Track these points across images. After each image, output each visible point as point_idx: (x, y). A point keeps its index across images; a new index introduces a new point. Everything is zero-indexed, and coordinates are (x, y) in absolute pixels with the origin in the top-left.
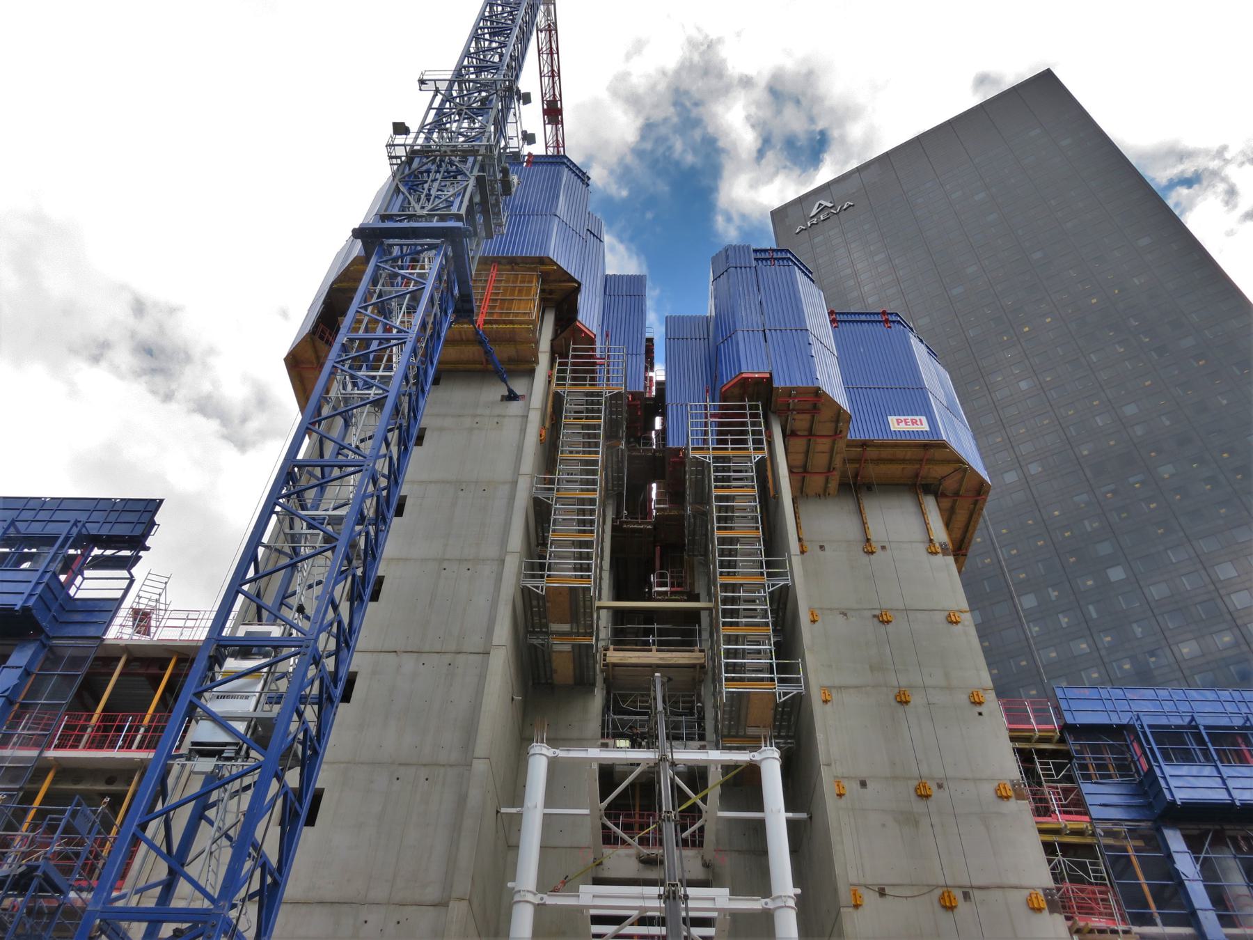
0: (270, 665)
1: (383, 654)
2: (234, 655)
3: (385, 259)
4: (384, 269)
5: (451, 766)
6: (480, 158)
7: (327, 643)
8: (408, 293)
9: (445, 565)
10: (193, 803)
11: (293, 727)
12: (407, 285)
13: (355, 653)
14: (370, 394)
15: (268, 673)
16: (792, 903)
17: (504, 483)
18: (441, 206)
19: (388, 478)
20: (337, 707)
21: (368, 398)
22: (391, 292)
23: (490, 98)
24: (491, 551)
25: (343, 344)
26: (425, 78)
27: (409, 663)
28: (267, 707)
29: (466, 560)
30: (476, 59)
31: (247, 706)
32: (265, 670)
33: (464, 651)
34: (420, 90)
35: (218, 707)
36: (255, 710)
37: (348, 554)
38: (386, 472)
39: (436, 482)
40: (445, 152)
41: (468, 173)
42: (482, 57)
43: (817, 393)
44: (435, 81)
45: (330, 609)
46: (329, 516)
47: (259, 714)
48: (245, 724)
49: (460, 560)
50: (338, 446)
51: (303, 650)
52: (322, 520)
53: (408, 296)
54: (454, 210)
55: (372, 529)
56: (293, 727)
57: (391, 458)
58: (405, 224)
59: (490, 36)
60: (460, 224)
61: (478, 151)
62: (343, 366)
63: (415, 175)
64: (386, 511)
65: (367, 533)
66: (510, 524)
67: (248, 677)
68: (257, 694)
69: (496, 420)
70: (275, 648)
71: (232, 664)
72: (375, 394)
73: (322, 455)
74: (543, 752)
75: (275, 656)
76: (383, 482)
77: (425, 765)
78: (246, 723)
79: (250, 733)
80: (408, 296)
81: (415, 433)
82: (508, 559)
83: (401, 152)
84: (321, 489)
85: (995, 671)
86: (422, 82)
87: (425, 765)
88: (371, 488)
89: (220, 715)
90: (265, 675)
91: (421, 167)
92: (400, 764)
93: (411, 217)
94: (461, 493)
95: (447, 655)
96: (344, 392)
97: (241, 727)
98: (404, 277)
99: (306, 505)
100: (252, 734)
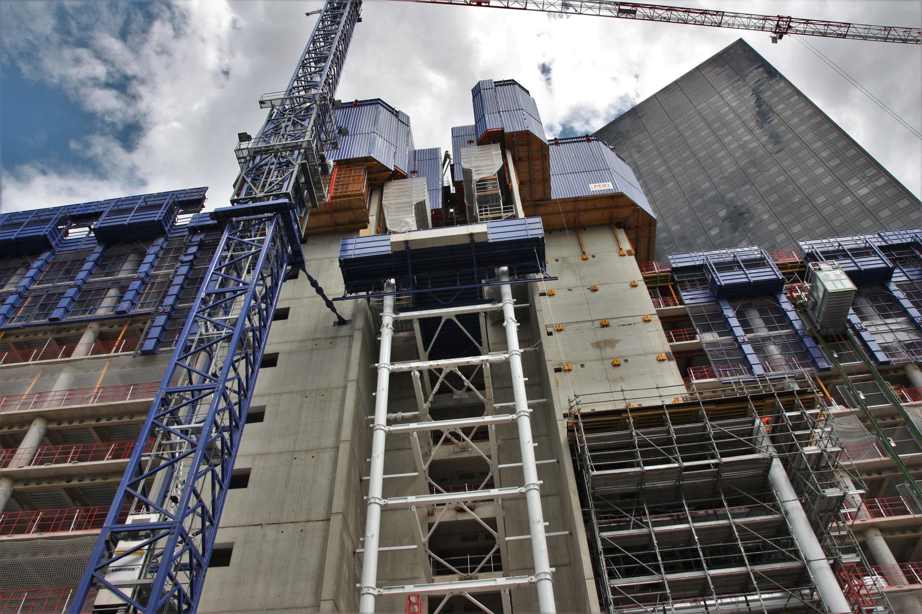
0: (150, 543)
1: (251, 527)
2: (125, 539)
3: (234, 232)
4: (234, 239)
5: (306, 607)
6: (302, 151)
7: (192, 523)
8: (250, 255)
9: (296, 455)
11: (168, 587)
12: (251, 249)
13: (219, 530)
14: (222, 333)
15: (149, 550)
17: (337, 388)
18: (275, 188)
20: (206, 571)
21: (220, 336)
22: (241, 255)
23: (312, 107)
24: (329, 441)
25: (202, 299)
26: (264, 99)
27: (271, 532)
28: (149, 576)
29: (311, 450)
30: (305, 81)
31: (132, 576)
32: (146, 547)
34: (261, 108)
35: (111, 578)
36: (139, 578)
37: (205, 454)
38: (236, 388)
39: (287, 393)
40: (278, 149)
41: (294, 163)
42: (309, 79)
44: (271, 101)
45: (193, 497)
46: (191, 428)
47: (142, 581)
48: (132, 589)
49: (306, 450)
50: (203, 377)
51: (172, 531)
53: (250, 257)
54: (284, 190)
56: (168, 587)
57: (239, 380)
58: (251, 204)
59: (315, 64)
60: (286, 200)
61: (301, 146)
62: (204, 314)
63: (259, 169)
66: (342, 419)
67: (134, 553)
68: (141, 566)
69: (330, 341)
70: (153, 530)
71: (123, 545)
72: (226, 333)
73: (191, 382)
74: (370, 592)
75: (153, 537)
76: (234, 398)
77: (286, 609)
78: (132, 589)
79: (136, 596)
80: (250, 257)
82: (342, 446)
83: (245, 153)
84: (193, 406)
85: (374, 394)
86: (262, 102)
87: (286, 609)
88: (223, 404)
89: (113, 584)
90: (146, 551)
91: (261, 162)
92: (268, 610)
93: (255, 200)
94: (306, 400)
95: (299, 524)
97: (128, 592)
98: (247, 244)
99: (180, 421)
100: (138, 597)
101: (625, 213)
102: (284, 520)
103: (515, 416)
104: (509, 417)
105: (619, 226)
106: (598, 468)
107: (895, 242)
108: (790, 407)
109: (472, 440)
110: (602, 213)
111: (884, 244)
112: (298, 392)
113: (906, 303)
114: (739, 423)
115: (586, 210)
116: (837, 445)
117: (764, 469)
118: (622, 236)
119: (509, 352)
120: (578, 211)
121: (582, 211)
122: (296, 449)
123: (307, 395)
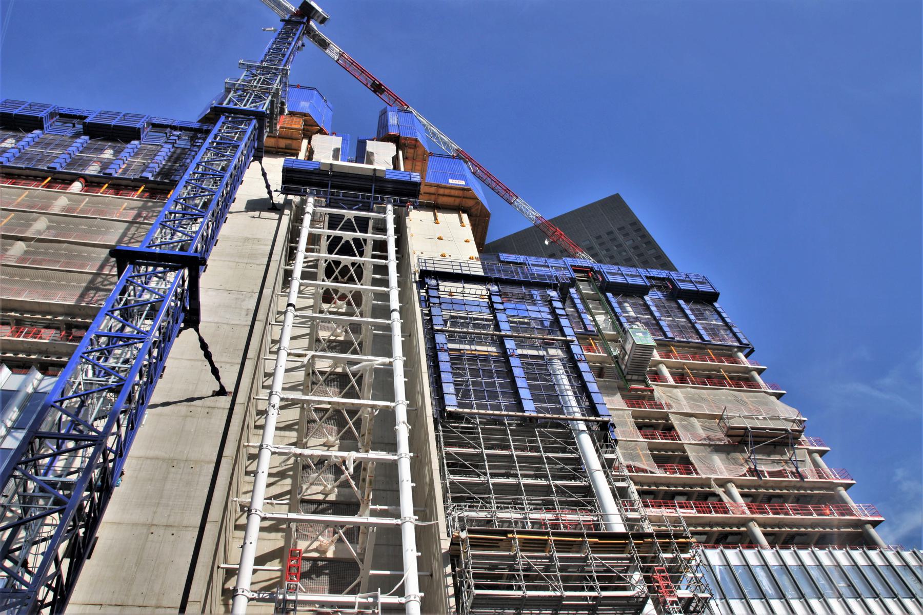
1: (89, 606)
9: (153, 529)
10: (11, 529)
16: (418, 599)
19: (115, 453)
33: (163, 605)
39: (151, 459)
43: (416, 140)
46: (61, 482)
49: (166, 526)
52: (53, 485)
53: (149, 305)
55: (97, 495)
64: (153, 375)
65: (93, 499)
69: (207, 410)
80: (149, 305)
81: (232, 198)
94: (173, 470)
96: (86, 378)
101: (470, 203)
102: (130, 603)
103: (399, 522)
104: (394, 521)
105: (464, 212)
106: (478, 587)
107: (656, 276)
108: (666, 548)
109: (353, 344)
110: (455, 200)
111: (648, 275)
112: (164, 460)
113: (653, 308)
114: (617, 559)
115: (444, 195)
116: (706, 591)
117: (637, 607)
118: (465, 217)
119: (398, 453)
120: (438, 195)
121: (441, 195)
122: (155, 522)
123: (175, 464)
